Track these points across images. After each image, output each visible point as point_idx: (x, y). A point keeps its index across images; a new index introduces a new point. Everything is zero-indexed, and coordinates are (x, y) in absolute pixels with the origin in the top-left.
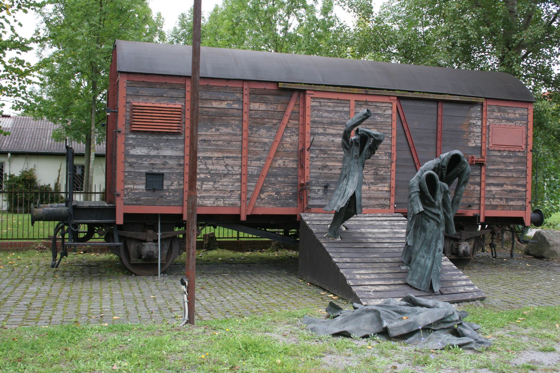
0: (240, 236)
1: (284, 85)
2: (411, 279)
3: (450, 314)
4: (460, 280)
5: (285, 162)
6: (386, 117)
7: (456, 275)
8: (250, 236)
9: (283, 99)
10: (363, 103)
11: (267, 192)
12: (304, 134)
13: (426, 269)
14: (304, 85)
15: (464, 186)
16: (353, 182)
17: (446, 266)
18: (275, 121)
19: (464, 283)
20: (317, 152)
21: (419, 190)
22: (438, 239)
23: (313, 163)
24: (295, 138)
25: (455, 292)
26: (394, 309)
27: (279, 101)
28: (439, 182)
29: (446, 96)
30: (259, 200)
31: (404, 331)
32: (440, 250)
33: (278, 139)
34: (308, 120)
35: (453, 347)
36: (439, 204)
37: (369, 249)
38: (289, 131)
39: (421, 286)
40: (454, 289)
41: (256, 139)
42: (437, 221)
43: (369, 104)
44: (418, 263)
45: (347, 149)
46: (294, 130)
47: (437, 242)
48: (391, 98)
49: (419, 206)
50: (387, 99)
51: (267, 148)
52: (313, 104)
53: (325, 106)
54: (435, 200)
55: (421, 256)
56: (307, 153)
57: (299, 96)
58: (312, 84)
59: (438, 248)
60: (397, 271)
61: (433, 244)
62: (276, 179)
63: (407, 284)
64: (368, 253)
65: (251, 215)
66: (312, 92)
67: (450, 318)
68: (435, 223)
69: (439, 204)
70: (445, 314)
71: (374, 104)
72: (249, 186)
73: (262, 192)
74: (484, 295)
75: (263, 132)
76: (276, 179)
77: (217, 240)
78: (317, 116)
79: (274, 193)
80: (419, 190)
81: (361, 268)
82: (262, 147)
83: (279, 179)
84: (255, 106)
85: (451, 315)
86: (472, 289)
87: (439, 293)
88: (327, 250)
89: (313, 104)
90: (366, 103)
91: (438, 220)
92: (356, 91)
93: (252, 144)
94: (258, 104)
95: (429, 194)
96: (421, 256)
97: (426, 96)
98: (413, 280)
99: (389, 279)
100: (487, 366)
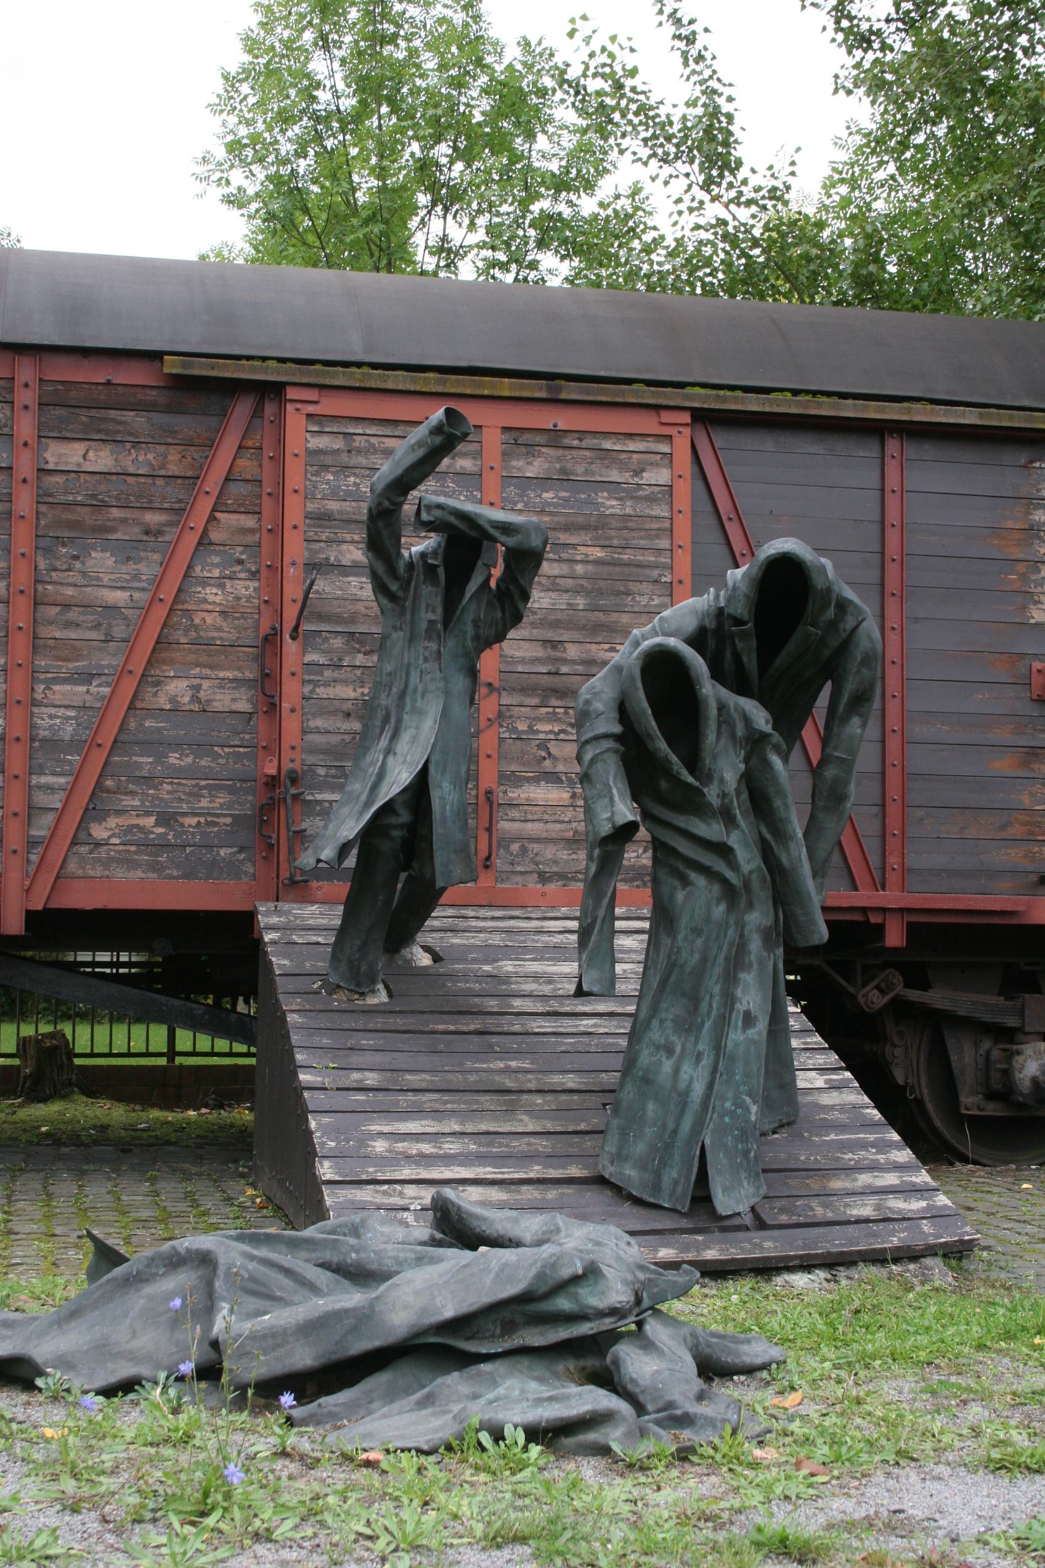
0: (179, 1048)
1: (184, 365)
2: (619, 1157)
3: (566, 1272)
4: (874, 1167)
5: (197, 688)
6: (647, 498)
7: (864, 1145)
8: (222, 1045)
9: (188, 425)
10: (539, 439)
11: (119, 813)
12: (276, 570)
13: (683, 1107)
14: (272, 364)
15: (856, 721)
16: (414, 740)
17: (832, 1108)
18: (153, 518)
19: (891, 1179)
20: (337, 643)
21: (617, 729)
22: (737, 962)
23: (321, 691)
24: (245, 588)
25: (830, 1215)
26: (328, 1256)
27: (173, 433)
28: (710, 690)
29: (918, 406)
30: (84, 849)
31: (303, 1357)
32: (749, 1020)
33: (168, 594)
34: (294, 511)
35: (498, 1436)
36: (724, 795)
37: (494, 1039)
38: (216, 560)
39: (657, 1187)
40: (825, 1206)
41: (70, 591)
42: (725, 882)
43: (567, 441)
44: (646, 1081)
45: (392, 597)
46: (238, 553)
47: (730, 978)
48: (667, 416)
49: (612, 800)
50: (646, 423)
51: (119, 631)
52: (315, 443)
53: (372, 450)
54: (707, 777)
55: (658, 1047)
56: (291, 647)
57: (257, 413)
58: (312, 362)
59: (740, 1007)
60: (582, 1127)
61: (714, 986)
62: (160, 758)
63: (601, 1181)
64: (490, 1052)
65: (46, 910)
66: (313, 395)
67: (575, 1297)
68: (716, 888)
69: (724, 795)
70: (541, 1276)
71: (589, 442)
72: (40, 787)
73: (94, 812)
74: (968, 1232)
75: (101, 561)
76: (160, 758)
77: (78, 1061)
78: (334, 495)
79: (152, 820)
80: (617, 729)
81: (417, 1113)
82: (97, 626)
83: (174, 759)
84: (67, 455)
85: (576, 1279)
86: (917, 1205)
87: (748, 1220)
88: (295, 1038)
89: (315, 443)
90: (555, 437)
91: (729, 874)
92: (506, 387)
93: (53, 611)
94: (79, 448)
95: (662, 745)
96: (658, 1047)
97: (825, 408)
98: (626, 1159)
99: (531, 1157)
100: (541, 1538)
